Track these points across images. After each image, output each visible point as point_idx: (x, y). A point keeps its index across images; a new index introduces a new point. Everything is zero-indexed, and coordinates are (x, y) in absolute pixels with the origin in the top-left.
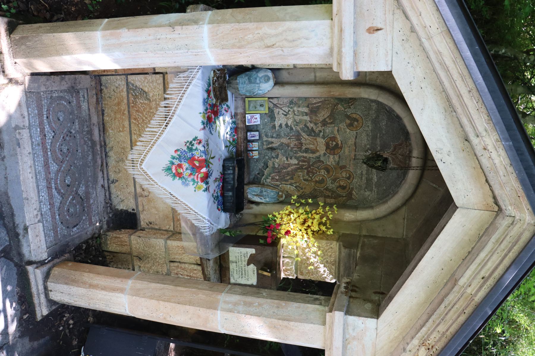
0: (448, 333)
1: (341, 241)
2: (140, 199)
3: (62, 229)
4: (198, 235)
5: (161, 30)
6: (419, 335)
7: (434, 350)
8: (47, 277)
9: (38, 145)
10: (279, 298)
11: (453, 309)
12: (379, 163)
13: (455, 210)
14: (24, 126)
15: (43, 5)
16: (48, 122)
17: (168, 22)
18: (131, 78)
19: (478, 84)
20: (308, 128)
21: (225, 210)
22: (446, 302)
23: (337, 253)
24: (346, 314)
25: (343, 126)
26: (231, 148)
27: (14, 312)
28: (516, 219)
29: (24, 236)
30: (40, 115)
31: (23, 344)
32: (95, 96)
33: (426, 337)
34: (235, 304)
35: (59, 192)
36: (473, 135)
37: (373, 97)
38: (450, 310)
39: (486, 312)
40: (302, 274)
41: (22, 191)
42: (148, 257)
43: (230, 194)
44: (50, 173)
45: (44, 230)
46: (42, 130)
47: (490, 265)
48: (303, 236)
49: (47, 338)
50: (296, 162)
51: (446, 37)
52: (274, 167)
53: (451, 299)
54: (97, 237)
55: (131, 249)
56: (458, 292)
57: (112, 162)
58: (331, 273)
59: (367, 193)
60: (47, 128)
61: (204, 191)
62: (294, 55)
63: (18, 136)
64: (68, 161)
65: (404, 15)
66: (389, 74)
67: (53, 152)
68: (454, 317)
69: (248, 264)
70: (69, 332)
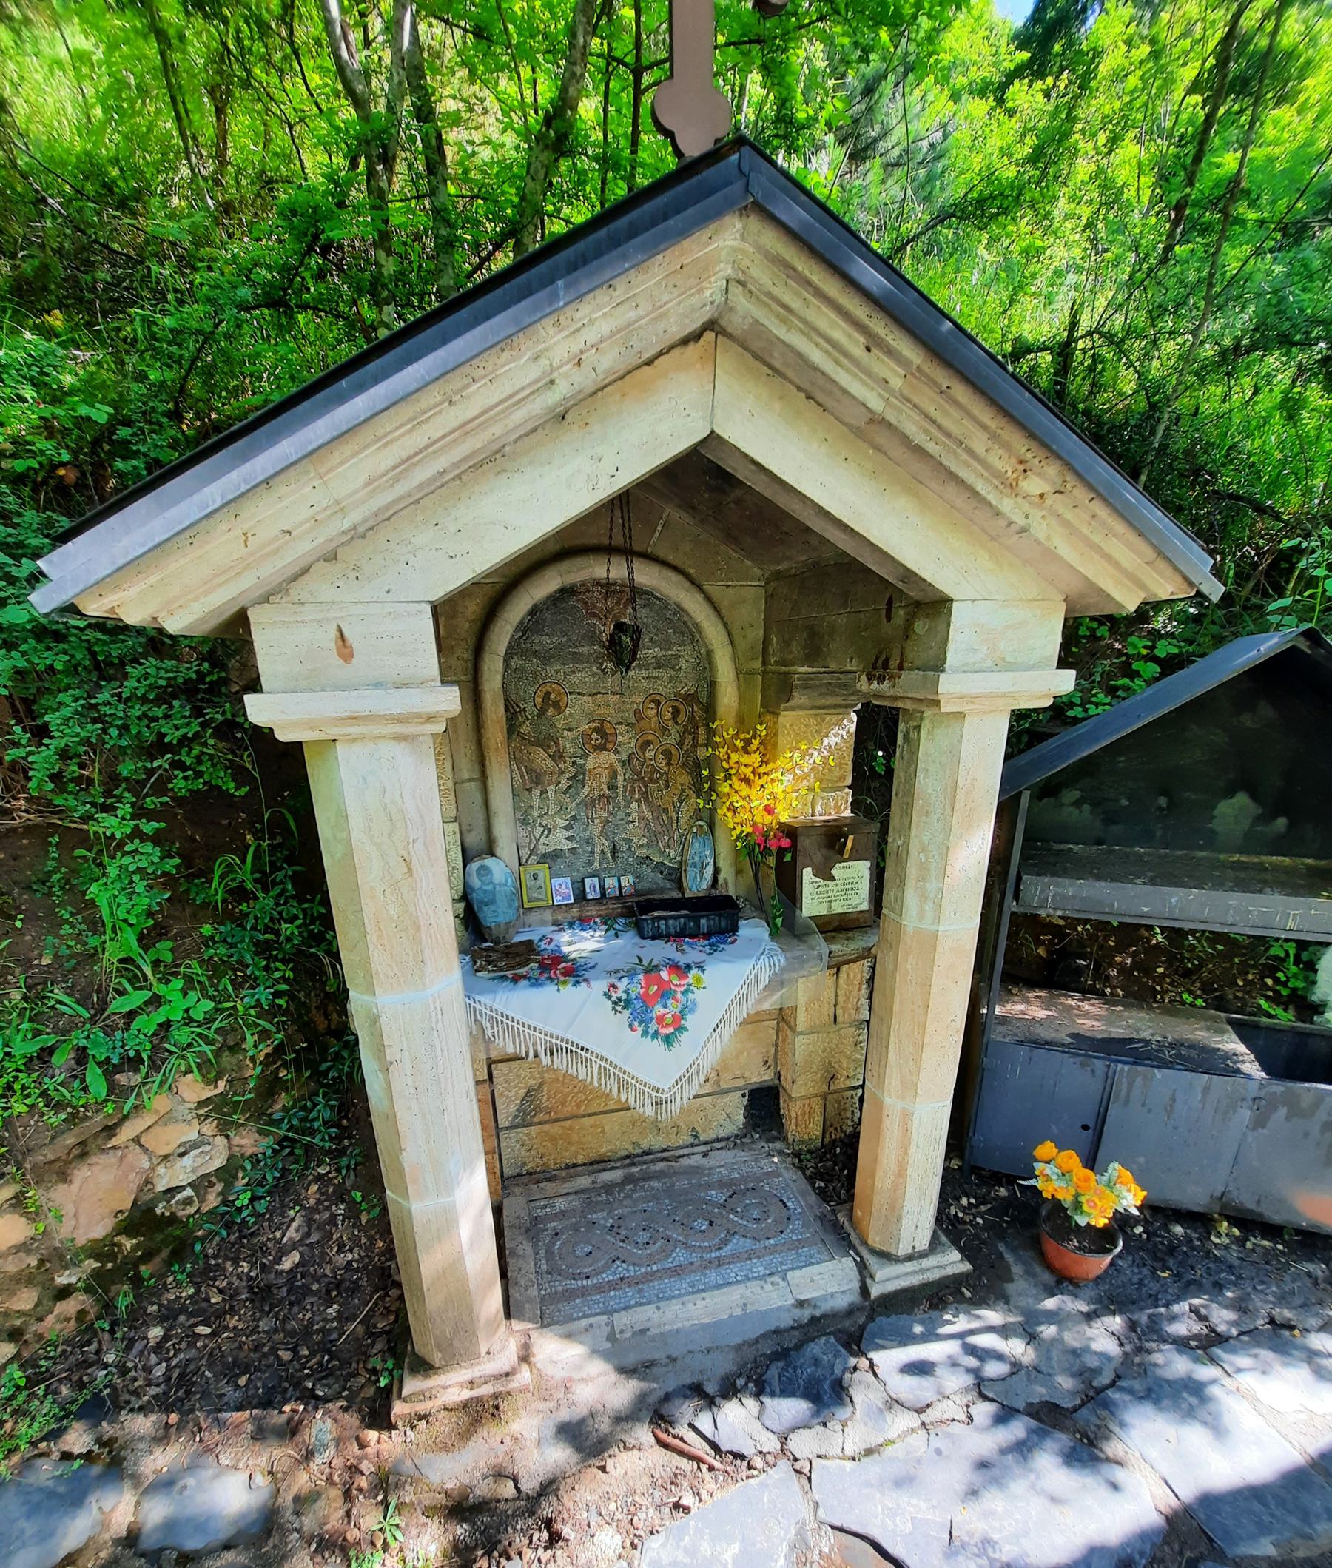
1: (778, 706)
2: (724, 1086)
3: (792, 1232)
4: (786, 976)
5: (396, 1086)
7: (1029, 455)
9: (640, 1291)
10: (908, 810)
11: (939, 420)
12: (626, 639)
13: (719, 437)
14: (607, 1324)
15: (376, 1304)
16: (597, 1274)
17: (380, 1075)
19: (428, 373)
20: (569, 787)
21: (734, 929)
22: (920, 439)
23: (801, 713)
24: (943, 671)
26: (618, 927)
27: (961, 1316)
28: (733, 276)
30: (583, 1292)
31: (1020, 1295)
32: (542, 1185)
33: (996, 482)
34: (924, 897)
35: (724, 1242)
36: (549, 394)
37: (499, 664)
39: (949, 332)
40: (843, 778)
41: (731, 1316)
42: (830, 1063)
43: (703, 921)
44: (692, 1263)
45: (801, 1268)
46: (612, 1286)
47: (840, 332)
48: (772, 780)
49: (1001, 1247)
50: (635, 804)
51: (329, 465)
52: (648, 845)
53: (914, 429)
54: (796, 1158)
55: (816, 1096)
56: (900, 411)
57: (659, 1142)
58: (839, 723)
60: (607, 1277)
61: (703, 971)
62: (422, 817)
63: (628, 1335)
64: (666, 1229)
65: (301, 579)
66: (436, 609)
67: (651, 1259)
68: (955, 413)
70: (984, 1204)
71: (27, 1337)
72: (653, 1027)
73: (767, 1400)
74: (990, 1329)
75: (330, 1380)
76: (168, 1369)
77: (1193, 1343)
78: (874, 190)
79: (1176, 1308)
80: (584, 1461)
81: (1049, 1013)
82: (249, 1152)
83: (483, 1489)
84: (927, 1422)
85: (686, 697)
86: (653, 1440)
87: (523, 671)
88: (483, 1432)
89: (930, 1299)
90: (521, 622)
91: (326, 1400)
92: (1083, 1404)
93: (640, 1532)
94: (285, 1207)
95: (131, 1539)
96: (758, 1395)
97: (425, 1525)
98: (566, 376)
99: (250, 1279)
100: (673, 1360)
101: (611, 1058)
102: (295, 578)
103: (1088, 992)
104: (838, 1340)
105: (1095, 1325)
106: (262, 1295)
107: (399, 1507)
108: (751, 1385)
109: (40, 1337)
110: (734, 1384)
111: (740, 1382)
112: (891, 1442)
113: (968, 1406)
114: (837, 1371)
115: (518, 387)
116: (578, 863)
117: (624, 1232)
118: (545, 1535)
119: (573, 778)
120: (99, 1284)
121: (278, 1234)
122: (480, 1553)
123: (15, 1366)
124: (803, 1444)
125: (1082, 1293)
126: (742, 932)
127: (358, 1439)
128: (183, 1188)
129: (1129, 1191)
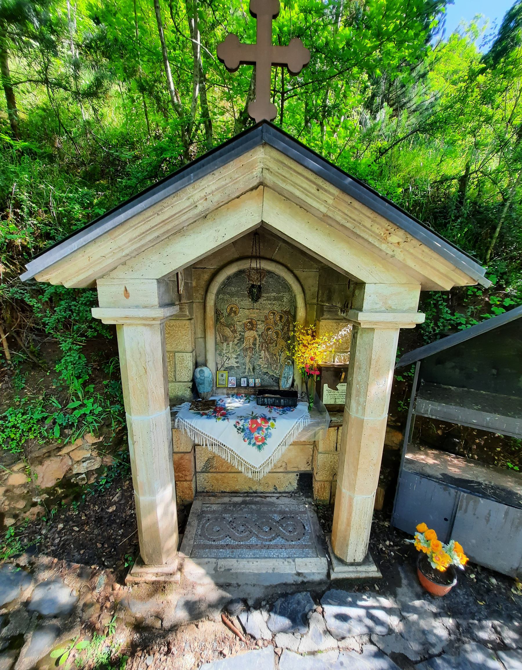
0: (372, 216)
3: (304, 540)
6: (376, 244)
7: (389, 228)
8: (342, 561)
9: (232, 552)
18: (198, 470)
21: (295, 405)
22: (343, 222)
25: (236, 319)
29: (305, 577)
30: (210, 547)
31: (403, 595)
34: (358, 403)
35: (274, 538)
38: (350, 217)
39: (350, 183)
40: (347, 348)
41: (267, 572)
43: (282, 401)
45: (302, 558)
46: (223, 547)
47: (306, 184)
49: (400, 569)
50: (263, 352)
52: (267, 368)
55: (327, 481)
56: (334, 212)
57: (260, 489)
58: (346, 326)
59: (285, 300)
60: (222, 543)
63: (222, 570)
66: (159, 281)
68: (357, 212)
69: (337, 390)
70: (397, 546)
71: (20, 518)
72: (253, 441)
73: (272, 615)
74: (384, 609)
75: (111, 559)
76: (60, 541)
77: (490, 645)
78: (404, 121)
79: (484, 623)
80: (190, 620)
81: (436, 462)
82: (109, 464)
83: (150, 621)
84: (340, 646)
85: (285, 312)
86: (221, 619)
87: (223, 299)
88: (157, 596)
89: (359, 586)
90: (224, 282)
91: (107, 567)
92: (421, 661)
93: (203, 660)
94: (116, 488)
95: (26, 604)
96: (269, 611)
97: (124, 629)
98: (201, 204)
99: (97, 513)
100: (239, 586)
101: (236, 451)
102: (112, 270)
103: (458, 454)
104: (311, 595)
105: (438, 620)
106: (99, 520)
107: (117, 619)
108: (267, 606)
109: (24, 519)
110: (260, 603)
111: (263, 603)
112: (321, 652)
113: (362, 644)
114: (307, 610)
115: (182, 208)
116: (240, 372)
117: (234, 525)
118: (166, 649)
119: (239, 340)
120: (47, 504)
121: (111, 498)
122: (139, 649)
123: (13, 527)
124: (283, 640)
125: (434, 602)
126: (298, 407)
127: (112, 586)
128: (82, 474)
129: (458, 556)
